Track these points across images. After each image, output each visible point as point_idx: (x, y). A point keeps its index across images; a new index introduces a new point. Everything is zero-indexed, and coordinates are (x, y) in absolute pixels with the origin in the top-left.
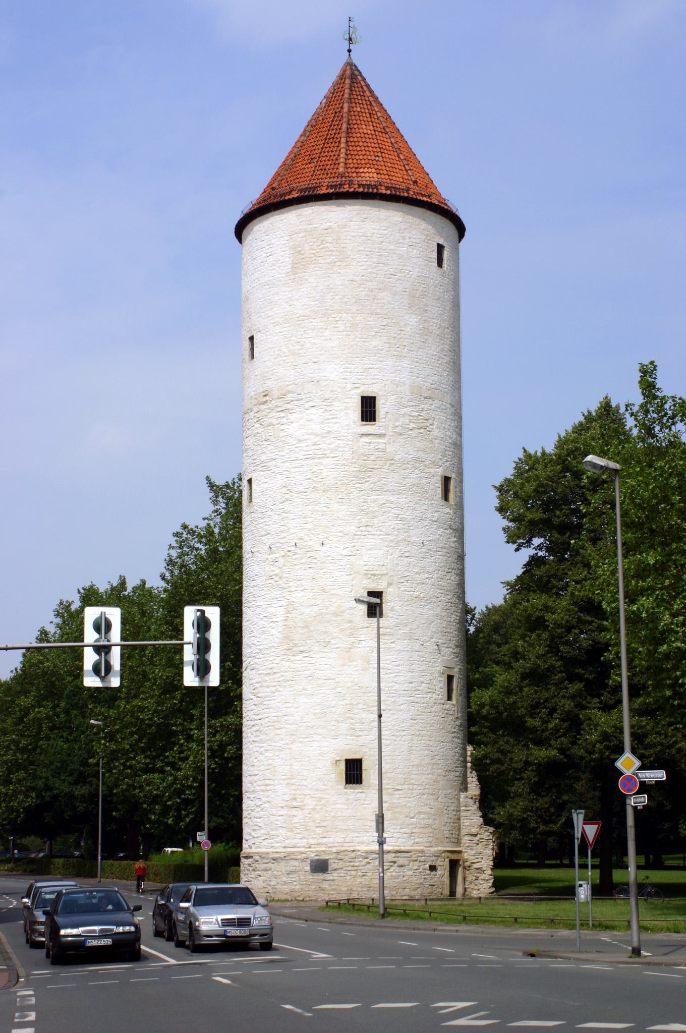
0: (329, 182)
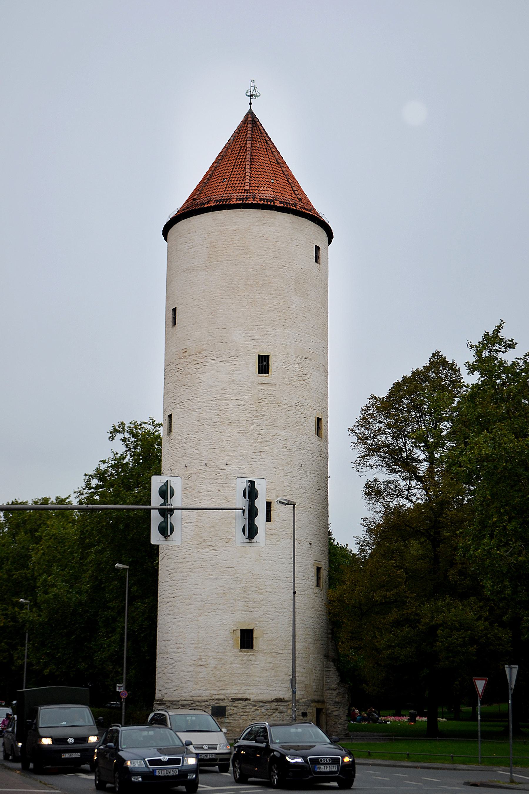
0: (238, 196)
